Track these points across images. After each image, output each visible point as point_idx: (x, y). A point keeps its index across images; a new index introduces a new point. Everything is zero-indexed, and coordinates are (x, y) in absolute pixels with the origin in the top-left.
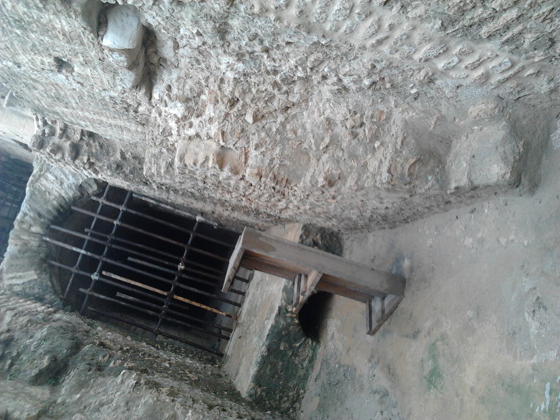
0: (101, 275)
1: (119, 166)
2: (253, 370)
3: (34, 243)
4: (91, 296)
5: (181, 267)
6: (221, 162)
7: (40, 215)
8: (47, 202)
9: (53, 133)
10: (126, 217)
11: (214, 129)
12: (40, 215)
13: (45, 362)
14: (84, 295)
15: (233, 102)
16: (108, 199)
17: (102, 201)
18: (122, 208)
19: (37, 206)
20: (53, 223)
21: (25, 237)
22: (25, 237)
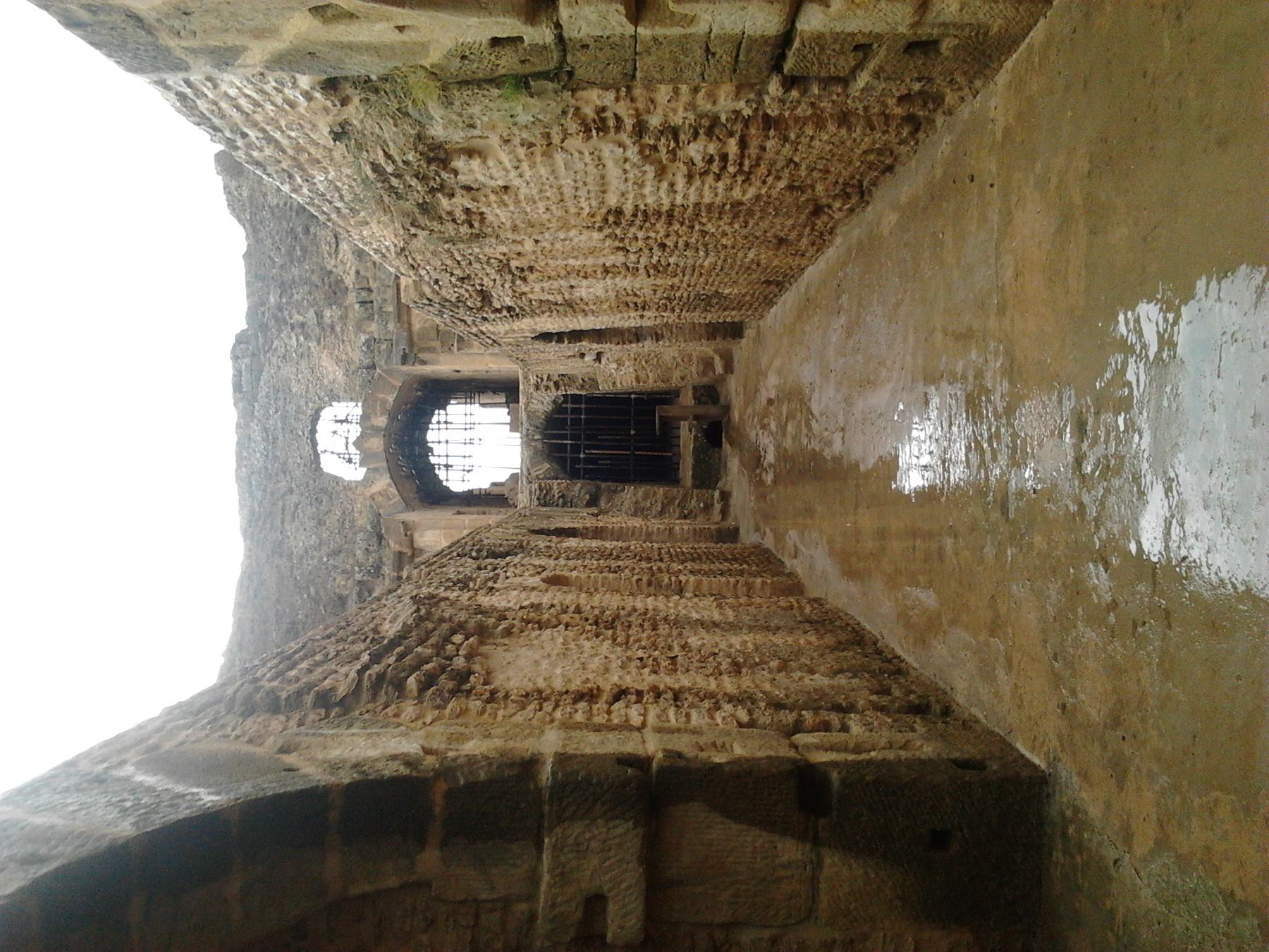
0: (585, 453)
1: (582, 386)
2: (690, 473)
3: (540, 446)
4: (585, 469)
5: (633, 432)
6: (638, 382)
7: (537, 428)
8: (539, 418)
9: (542, 379)
10: (588, 411)
11: (631, 370)
12: (537, 428)
13: (588, 497)
14: (579, 469)
15: (635, 360)
16: (572, 403)
17: (569, 405)
18: (583, 406)
19: (534, 422)
20: (546, 429)
21: (534, 444)
22: (534, 444)
